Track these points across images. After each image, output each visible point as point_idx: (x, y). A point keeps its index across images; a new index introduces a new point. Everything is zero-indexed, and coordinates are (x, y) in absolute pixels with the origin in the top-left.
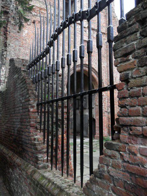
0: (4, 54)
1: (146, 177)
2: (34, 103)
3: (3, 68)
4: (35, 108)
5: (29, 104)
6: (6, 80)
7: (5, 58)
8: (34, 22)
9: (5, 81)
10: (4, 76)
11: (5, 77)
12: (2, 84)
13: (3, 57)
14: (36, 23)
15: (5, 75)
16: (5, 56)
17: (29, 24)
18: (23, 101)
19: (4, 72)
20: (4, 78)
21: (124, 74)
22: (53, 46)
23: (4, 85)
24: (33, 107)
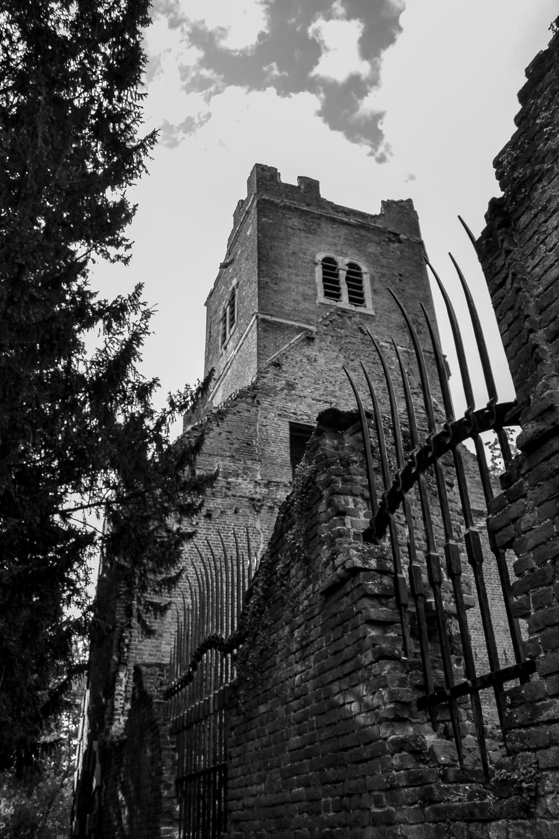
0: (126, 637)
1: (33, 837)
2: (170, 779)
3: (122, 675)
4: (173, 789)
5: (162, 782)
6: (128, 706)
7: (128, 646)
8: (209, 516)
9: (126, 708)
10: (124, 695)
11: (126, 700)
12: (117, 717)
13: (122, 644)
14: (215, 516)
15: (125, 691)
16: (127, 641)
17: (194, 523)
18: (153, 774)
19: (123, 686)
20: (122, 702)
21: (543, 590)
22: (477, 244)
23: (122, 721)
24: (168, 787)
